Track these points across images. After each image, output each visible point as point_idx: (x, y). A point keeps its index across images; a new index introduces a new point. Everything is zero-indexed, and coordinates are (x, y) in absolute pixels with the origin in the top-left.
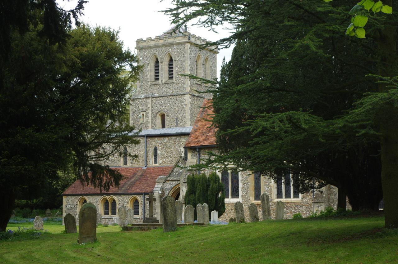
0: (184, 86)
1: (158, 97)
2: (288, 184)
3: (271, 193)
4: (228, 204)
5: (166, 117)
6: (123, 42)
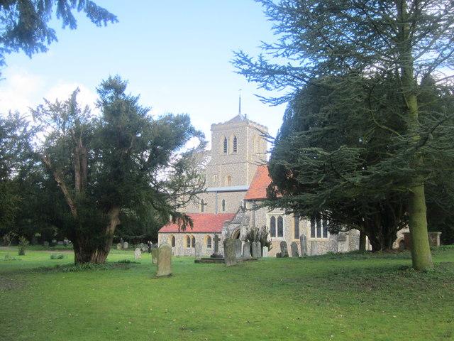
2: (319, 226)
3: (307, 233)
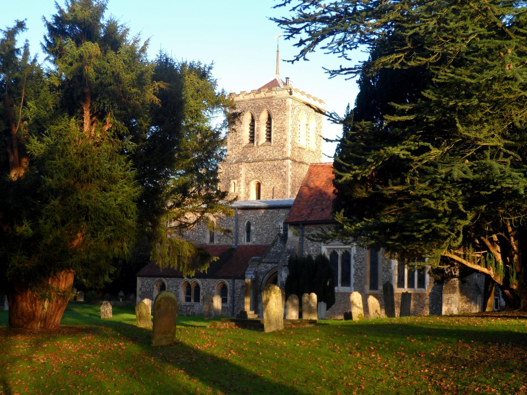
0: (284, 150)
1: (252, 162)
4: (337, 293)
5: (262, 186)
6: (216, 82)
